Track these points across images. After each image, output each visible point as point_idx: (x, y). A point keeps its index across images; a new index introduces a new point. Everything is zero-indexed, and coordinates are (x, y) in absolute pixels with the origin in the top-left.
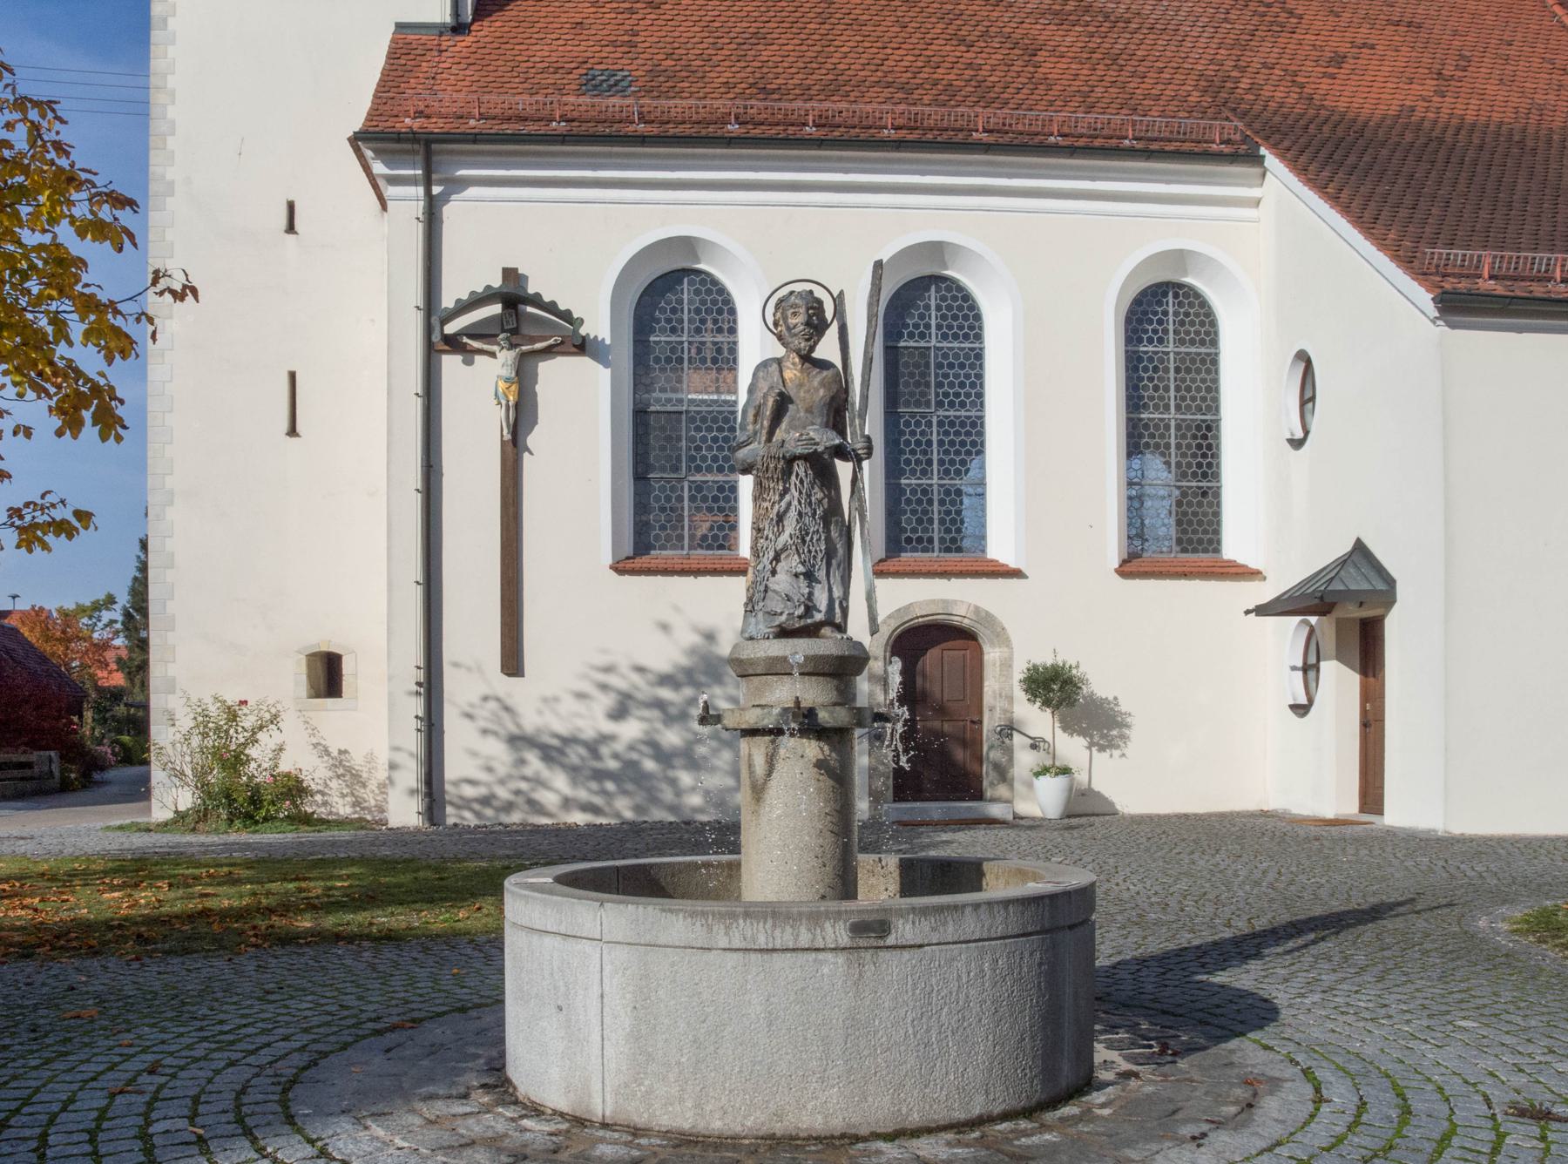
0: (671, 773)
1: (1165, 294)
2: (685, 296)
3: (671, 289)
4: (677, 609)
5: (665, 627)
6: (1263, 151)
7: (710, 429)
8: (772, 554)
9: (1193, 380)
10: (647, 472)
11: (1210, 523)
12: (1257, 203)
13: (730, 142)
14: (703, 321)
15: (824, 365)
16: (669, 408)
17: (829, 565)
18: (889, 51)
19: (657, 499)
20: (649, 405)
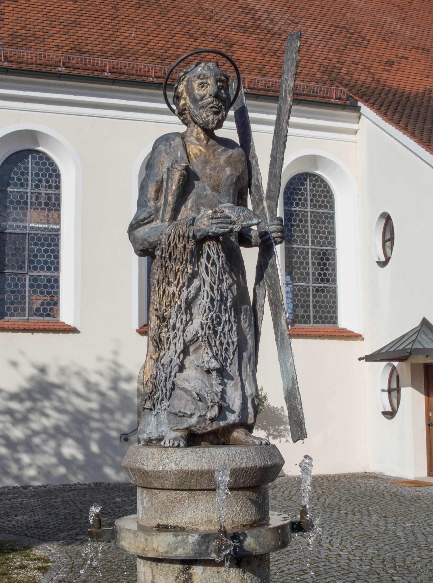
0: (16, 455)
1: (305, 180)
2: (30, 166)
3: (21, 161)
4: (22, 353)
5: (14, 364)
6: (359, 104)
7: (43, 245)
8: (180, 347)
9: (321, 228)
10: (3, 269)
11: (331, 307)
12: (355, 132)
13: (59, 76)
14: (40, 181)
15: (226, 143)
16: (18, 231)
17: (240, 358)
18: (151, 38)
19: (9, 285)
20: (6, 229)
